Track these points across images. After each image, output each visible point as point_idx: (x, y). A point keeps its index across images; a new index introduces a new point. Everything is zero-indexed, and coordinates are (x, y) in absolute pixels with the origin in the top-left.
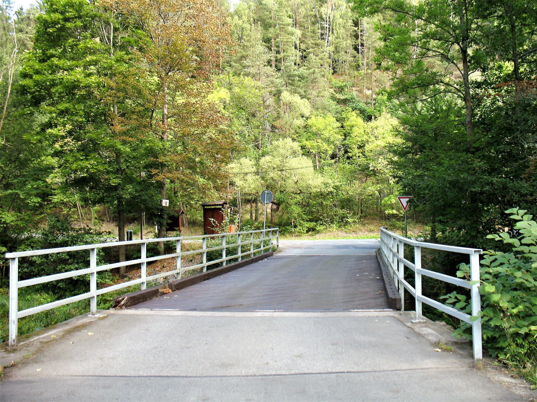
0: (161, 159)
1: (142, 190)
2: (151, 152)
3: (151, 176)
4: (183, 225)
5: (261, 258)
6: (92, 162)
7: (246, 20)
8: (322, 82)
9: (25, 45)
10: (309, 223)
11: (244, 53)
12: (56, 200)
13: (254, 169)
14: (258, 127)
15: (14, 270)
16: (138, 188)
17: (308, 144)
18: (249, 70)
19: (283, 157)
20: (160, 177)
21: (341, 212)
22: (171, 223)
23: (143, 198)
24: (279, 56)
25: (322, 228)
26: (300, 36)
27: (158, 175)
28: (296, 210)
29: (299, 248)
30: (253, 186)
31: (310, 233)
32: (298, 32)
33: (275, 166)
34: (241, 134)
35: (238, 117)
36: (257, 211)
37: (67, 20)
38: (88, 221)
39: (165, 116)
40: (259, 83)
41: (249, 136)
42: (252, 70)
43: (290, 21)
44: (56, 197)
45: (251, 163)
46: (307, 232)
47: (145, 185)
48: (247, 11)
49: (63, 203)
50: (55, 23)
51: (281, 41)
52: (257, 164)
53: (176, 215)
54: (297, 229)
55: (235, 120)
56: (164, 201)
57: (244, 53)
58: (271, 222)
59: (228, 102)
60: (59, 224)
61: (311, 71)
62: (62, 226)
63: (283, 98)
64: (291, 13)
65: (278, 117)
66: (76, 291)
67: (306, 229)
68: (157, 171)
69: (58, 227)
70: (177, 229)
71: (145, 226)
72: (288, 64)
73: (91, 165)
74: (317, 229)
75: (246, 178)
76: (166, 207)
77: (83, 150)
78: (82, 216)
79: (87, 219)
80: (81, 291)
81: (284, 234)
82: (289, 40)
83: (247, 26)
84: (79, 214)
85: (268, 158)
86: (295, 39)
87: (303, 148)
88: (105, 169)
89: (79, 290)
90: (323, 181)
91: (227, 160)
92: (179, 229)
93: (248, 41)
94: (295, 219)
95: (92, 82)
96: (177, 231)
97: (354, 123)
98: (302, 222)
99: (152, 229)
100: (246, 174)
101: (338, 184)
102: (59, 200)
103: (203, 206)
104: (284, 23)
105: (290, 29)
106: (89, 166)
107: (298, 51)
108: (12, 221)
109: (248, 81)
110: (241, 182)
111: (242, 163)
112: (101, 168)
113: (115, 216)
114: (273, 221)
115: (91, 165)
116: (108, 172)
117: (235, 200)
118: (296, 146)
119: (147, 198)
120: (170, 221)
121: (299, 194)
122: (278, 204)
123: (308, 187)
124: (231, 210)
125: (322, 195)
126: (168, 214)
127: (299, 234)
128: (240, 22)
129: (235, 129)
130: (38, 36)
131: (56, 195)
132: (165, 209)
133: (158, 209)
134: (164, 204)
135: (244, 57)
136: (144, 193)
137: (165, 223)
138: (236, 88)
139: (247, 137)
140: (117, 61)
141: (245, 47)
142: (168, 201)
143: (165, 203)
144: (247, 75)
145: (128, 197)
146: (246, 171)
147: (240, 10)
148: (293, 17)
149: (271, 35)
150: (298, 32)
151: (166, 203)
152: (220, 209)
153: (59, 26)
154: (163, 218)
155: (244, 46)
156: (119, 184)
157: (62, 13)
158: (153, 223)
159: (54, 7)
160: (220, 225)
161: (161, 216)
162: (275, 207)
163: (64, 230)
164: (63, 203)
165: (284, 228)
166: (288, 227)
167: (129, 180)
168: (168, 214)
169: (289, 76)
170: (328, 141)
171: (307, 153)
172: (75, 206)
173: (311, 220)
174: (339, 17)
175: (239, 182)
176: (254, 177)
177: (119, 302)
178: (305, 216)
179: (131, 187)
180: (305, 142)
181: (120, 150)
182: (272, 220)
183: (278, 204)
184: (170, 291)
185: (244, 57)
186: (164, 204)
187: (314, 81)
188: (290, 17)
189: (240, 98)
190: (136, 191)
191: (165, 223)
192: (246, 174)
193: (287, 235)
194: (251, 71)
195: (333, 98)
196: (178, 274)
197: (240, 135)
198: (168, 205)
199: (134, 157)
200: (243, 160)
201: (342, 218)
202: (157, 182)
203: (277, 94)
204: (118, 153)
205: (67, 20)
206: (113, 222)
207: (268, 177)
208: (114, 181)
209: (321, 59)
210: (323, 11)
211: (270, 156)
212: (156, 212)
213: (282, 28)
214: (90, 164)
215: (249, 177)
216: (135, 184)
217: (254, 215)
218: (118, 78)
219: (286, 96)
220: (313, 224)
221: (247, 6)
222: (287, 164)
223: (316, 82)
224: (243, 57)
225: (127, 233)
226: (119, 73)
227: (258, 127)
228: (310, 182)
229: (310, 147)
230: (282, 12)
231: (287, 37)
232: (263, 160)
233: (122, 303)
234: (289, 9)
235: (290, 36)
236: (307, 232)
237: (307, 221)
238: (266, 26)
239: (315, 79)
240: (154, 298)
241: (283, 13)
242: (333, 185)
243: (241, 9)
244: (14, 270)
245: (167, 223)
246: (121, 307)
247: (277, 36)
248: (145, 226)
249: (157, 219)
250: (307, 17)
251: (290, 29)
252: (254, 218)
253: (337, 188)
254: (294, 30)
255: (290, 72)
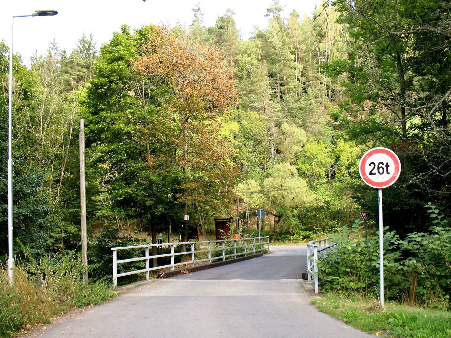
0: (183, 186)
1: (169, 209)
2: (176, 181)
3: (176, 199)
4: (202, 234)
5: (253, 257)
6: (133, 189)
7: (254, 57)
8: (319, 111)
9: (69, 85)
10: (305, 232)
11: (252, 88)
12: (99, 214)
13: (259, 188)
14: (263, 153)
15: (115, 255)
16: (166, 207)
17: (303, 167)
18: (255, 105)
19: (283, 178)
20: (183, 200)
21: (330, 222)
22: (191, 233)
23: (170, 214)
24: (283, 88)
25: (315, 235)
26: (301, 70)
27: (181, 198)
28: (295, 221)
29: (284, 251)
30: (258, 202)
31: (305, 240)
32: (300, 66)
33: (276, 186)
34: (248, 159)
35: (245, 145)
36: (263, 222)
37: (111, 82)
38: (125, 231)
39: (186, 153)
40: (263, 116)
41: (255, 160)
42: (257, 105)
43: (292, 57)
44: (99, 212)
45: (256, 183)
46: (303, 239)
47: (171, 205)
48: (255, 49)
49: (105, 217)
50: (103, 85)
51: (285, 75)
52: (261, 186)
53: (195, 226)
54: (295, 237)
55: (243, 147)
56: (186, 216)
57: (252, 88)
58: (274, 232)
59: (237, 133)
60: (109, 234)
61: (309, 102)
62: (112, 235)
63: (283, 129)
64: (293, 50)
65: (280, 143)
66: (123, 282)
67: (302, 237)
68: (180, 195)
69: (109, 236)
70: (195, 237)
71: (171, 235)
72: (288, 99)
73: (132, 191)
74: (311, 237)
75: (253, 195)
76: (187, 221)
77: (125, 180)
78: (120, 227)
79: (125, 230)
80: (126, 282)
81: (284, 241)
82: (291, 74)
83: (255, 62)
84: (117, 226)
85: (270, 179)
86: (297, 73)
87: (299, 170)
88: (142, 194)
89: (125, 281)
90: (315, 197)
91: (233, 185)
92: (197, 238)
93: (255, 77)
94: (293, 228)
95: (132, 129)
96: (195, 239)
97: (342, 148)
98: (298, 231)
99: (177, 238)
100: (252, 193)
101: (328, 200)
102: (101, 214)
103: (215, 220)
104: (287, 59)
105: (293, 64)
106: (131, 192)
107: (300, 83)
108: (75, 231)
109: (254, 115)
110: (248, 200)
111: (249, 183)
112: (139, 193)
113: (147, 227)
114: (276, 231)
115: (132, 191)
116: (145, 196)
117: (245, 213)
118: (293, 168)
119: (173, 214)
120: (190, 231)
121: (296, 208)
122: (280, 217)
123: (303, 202)
124: (242, 221)
125: (320, 209)
126: (189, 226)
127: (296, 241)
128: (249, 59)
129: (243, 155)
130: (90, 93)
131: (99, 210)
132: (186, 222)
133: (181, 222)
134: (185, 219)
135: (252, 91)
136: (171, 211)
137: (186, 233)
138: (244, 121)
139: (253, 162)
140: (149, 112)
141: (253, 83)
142: (189, 216)
143: (187, 218)
144: (252, 108)
145: (159, 214)
146: (253, 190)
147: (249, 49)
148: (295, 52)
149: (275, 70)
150: (300, 66)
151: (187, 218)
152: (226, 222)
153: (106, 87)
154: (185, 229)
155: (252, 81)
156: (152, 205)
157: (107, 77)
158: (178, 233)
159: (102, 73)
160: (227, 234)
161: (184, 228)
162: (277, 219)
163: (113, 238)
164: (105, 217)
165: (284, 236)
166: (287, 236)
167: (160, 201)
168: (189, 226)
169: (289, 109)
170: (320, 164)
171: (302, 174)
172: (115, 219)
173: (306, 230)
174: (335, 51)
175: (246, 199)
176: (258, 195)
177: (160, 275)
178: (301, 226)
179: (161, 206)
180: (301, 166)
181: (152, 180)
182: (274, 229)
183: (280, 217)
184: (188, 272)
185: (252, 91)
186: (185, 219)
187: (311, 111)
188: (292, 52)
189: (248, 129)
190: (165, 210)
191: (186, 233)
192: (252, 193)
193: (287, 242)
194: (257, 106)
195: (329, 124)
196: (192, 263)
197: (248, 161)
198: (189, 219)
199: (163, 185)
200: (250, 181)
201: (332, 227)
202: (180, 203)
203: (279, 125)
204: (151, 182)
205: (111, 82)
206: (145, 232)
207: (270, 195)
208: (149, 203)
209: (319, 90)
210: (321, 47)
211: (272, 178)
212: (179, 224)
213: (286, 63)
214: (131, 190)
215: (255, 196)
216: (164, 204)
217: (260, 226)
218: (151, 126)
219: (285, 126)
220: (307, 233)
221: (254, 45)
222: (285, 184)
223: (312, 112)
224: (251, 92)
225: (158, 240)
226: (151, 122)
227: (263, 153)
228: (305, 199)
229: (305, 169)
230: (285, 50)
231: (290, 71)
232: (266, 180)
233: (162, 276)
234: (292, 46)
235: (292, 70)
236: (303, 239)
237: (304, 230)
238: (273, 62)
239: (312, 109)
240: (178, 275)
241: (286, 51)
242: (323, 200)
243: (249, 47)
244: (115, 255)
245: (188, 233)
246: (161, 278)
247: (281, 70)
248: (171, 235)
249: (180, 230)
250: (309, 51)
251: (293, 64)
252: (260, 229)
253: (327, 203)
254: (296, 64)
255: (289, 105)
